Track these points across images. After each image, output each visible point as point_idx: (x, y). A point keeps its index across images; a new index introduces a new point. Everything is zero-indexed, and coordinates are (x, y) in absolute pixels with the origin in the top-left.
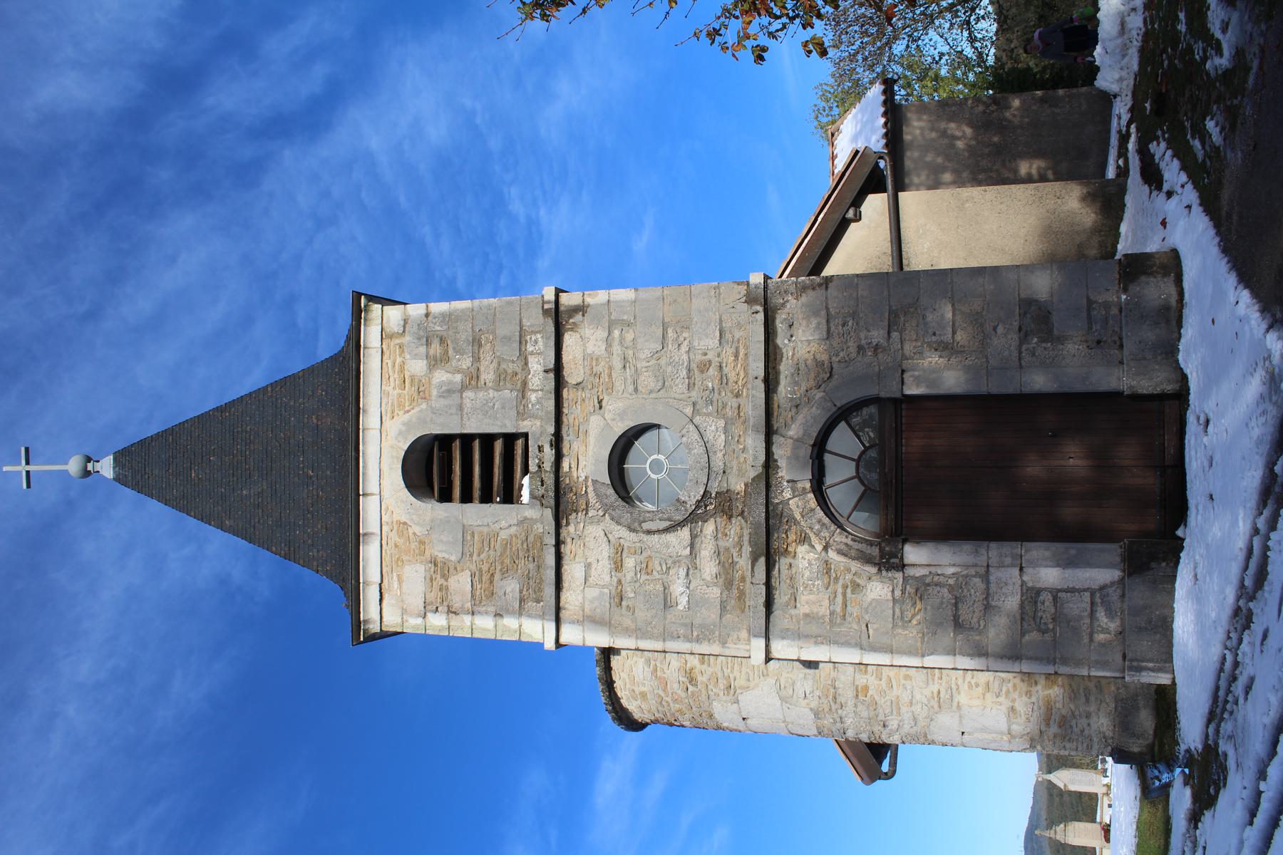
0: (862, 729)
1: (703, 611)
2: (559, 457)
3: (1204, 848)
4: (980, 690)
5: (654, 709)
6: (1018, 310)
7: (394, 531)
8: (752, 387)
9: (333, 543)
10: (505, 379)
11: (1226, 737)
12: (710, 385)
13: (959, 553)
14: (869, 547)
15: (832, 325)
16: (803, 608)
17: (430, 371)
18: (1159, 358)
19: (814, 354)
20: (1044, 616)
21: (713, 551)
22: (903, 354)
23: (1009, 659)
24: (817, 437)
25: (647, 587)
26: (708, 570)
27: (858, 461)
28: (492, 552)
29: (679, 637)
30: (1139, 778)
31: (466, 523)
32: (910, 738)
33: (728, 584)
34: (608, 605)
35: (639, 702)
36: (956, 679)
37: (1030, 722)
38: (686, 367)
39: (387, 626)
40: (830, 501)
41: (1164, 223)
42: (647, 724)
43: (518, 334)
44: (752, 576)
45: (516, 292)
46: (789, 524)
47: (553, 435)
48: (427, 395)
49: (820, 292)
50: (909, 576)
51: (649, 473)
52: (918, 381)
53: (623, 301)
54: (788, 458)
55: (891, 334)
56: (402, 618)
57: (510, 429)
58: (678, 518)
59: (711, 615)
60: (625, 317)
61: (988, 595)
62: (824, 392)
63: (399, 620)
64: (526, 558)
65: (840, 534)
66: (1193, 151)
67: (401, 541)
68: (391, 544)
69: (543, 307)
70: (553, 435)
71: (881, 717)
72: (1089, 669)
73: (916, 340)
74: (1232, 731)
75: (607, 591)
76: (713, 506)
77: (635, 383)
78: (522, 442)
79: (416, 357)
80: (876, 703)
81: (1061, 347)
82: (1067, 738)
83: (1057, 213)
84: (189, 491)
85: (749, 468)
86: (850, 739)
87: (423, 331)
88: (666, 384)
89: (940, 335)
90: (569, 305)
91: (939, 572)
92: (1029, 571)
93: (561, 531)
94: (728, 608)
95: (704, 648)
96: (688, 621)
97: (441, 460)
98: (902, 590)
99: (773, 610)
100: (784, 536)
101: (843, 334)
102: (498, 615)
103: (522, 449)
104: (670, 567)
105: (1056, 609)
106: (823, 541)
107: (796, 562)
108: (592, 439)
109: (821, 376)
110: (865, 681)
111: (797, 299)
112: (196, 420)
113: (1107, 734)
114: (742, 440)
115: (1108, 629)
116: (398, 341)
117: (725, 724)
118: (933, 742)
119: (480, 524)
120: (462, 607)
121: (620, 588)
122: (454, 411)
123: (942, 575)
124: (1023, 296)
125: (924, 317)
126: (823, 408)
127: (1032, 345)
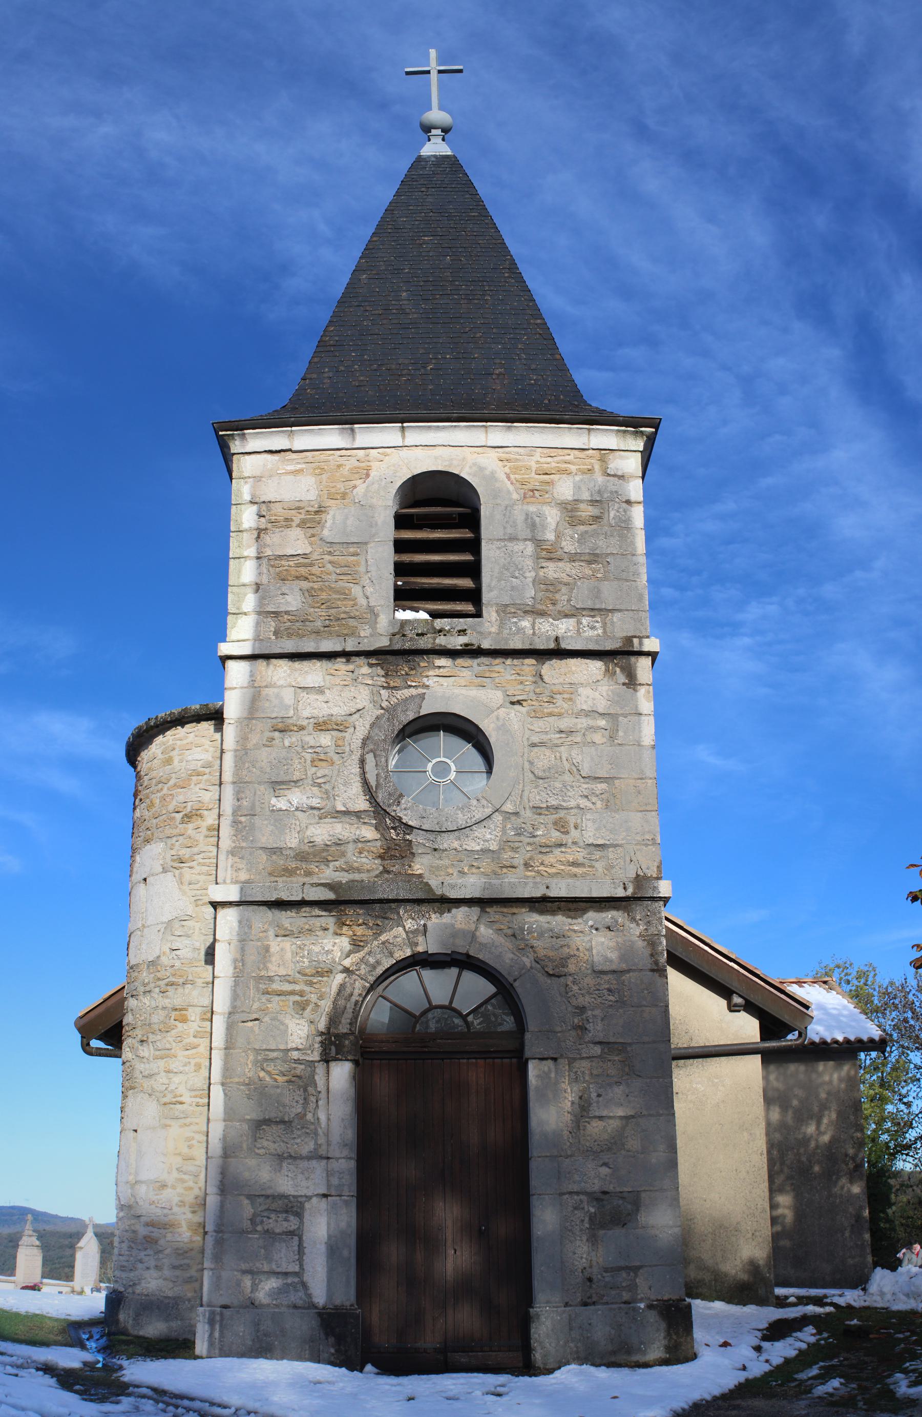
0: (138, 1016)
1: (271, 828)
2: (452, 654)
3: (17, 1375)
4: (185, 1150)
5: (153, 774)
6: (627, 1190)
7: (357, 464)
8: (536, 883)
9: (341, 395)
10: (547, 590)
11: (137, 1404)
12: (539, 833)
13: (342, 1126)
14: (349, 1021)
15: (610, 976)
16: (275, 945)
17: (559, 504)
18: (572, 1345)
19: (575, 955)
20: (271, 1221)
21: (341, 837)
22: (575, 1059)
23: (221, 1181)
24: (478, 959)
25: (296, 761)
26: (319, 831)
27: (449, 1008)
28: (334, 577)
29: (238, 800)
30: (90, 1319)
31: (369, 546)
32: (129, 1070)
33: (302, 856)
34: (274, 715)
35: (160, 756)
36: (197, 1124)
37: (150, 1205)
38: (561, 805)
39: (239, 460)
40: (402, 975)
41: (725, 1344)
42: (135, 767)
43: (603, 607)
44: (312, 885)
45: (654, 606)
46: (375, 927)
47: (479, 647)
48: (528, 500)
49: (647, 963)
50: (315, 1068)
51: (434, 761)
52: (542, 1077)
53: (640, 732)
54: (453, 925)
55: (599, 1046)
56: (249, 477)
57: (486, 596)
58: (380, 796)
59: (266, 838)
60: (621, 733)
61: (293, 1158)
62: (531, 967)
63: (246, 474)
64: (327, 618)
65: (364, 987)
66: (806, 1369)
67: (345, 471)
68: (342, 461)
69: (635, 637)
70: (479, 647)
71: (152, 1038)
72: (212, 1269)
73: (592, 1074)
74: (143, 1410)
75: (291, 713)
76: (394, 837)
77: (542, 744)
78: (470, 611)
79: (577, 488)
80: (168, 1032)
81: (585, 1238)
82: (133, 1245)
83: (736, 1233)
84: (404, 234)
85: (441, 879)
86: (126, 1003)
87: (608, 497)
88: (541, 781)
89: (598, 1102)
90: (636, 667)
91: (320, 1103)
92: (323, 1204)
93: (362, 658)
94: (274, 857)
95: (226, 831)
96: (258, 810)
97: (449, 516)
98: (299, 1060)
99: (273, 910)
100: (361, 921)
101: (599, 990)
102: (258, 587)
103: (462, 611)
104: (321, 787)
105: (279, 1234)
106: (355, 968)
107: (330, 936)
108: (474, 692)
109: (550, 964)
110: (193, 1019)
111: (641, 936)
112: (499, 241)
113: (138, 1287)
114: (474, 870)
115: (257, 1290)
116: (597, 467)
117: (138, 858)
118: (125, 1096)
119: (369, 563)
120: (265, 546)
121: (295, 728)
122: (509, 530)
123: (317, 1106)
124: (643, 1195)
125: (618, 1083)
126: (511, 966)
127: (586, 1207)
